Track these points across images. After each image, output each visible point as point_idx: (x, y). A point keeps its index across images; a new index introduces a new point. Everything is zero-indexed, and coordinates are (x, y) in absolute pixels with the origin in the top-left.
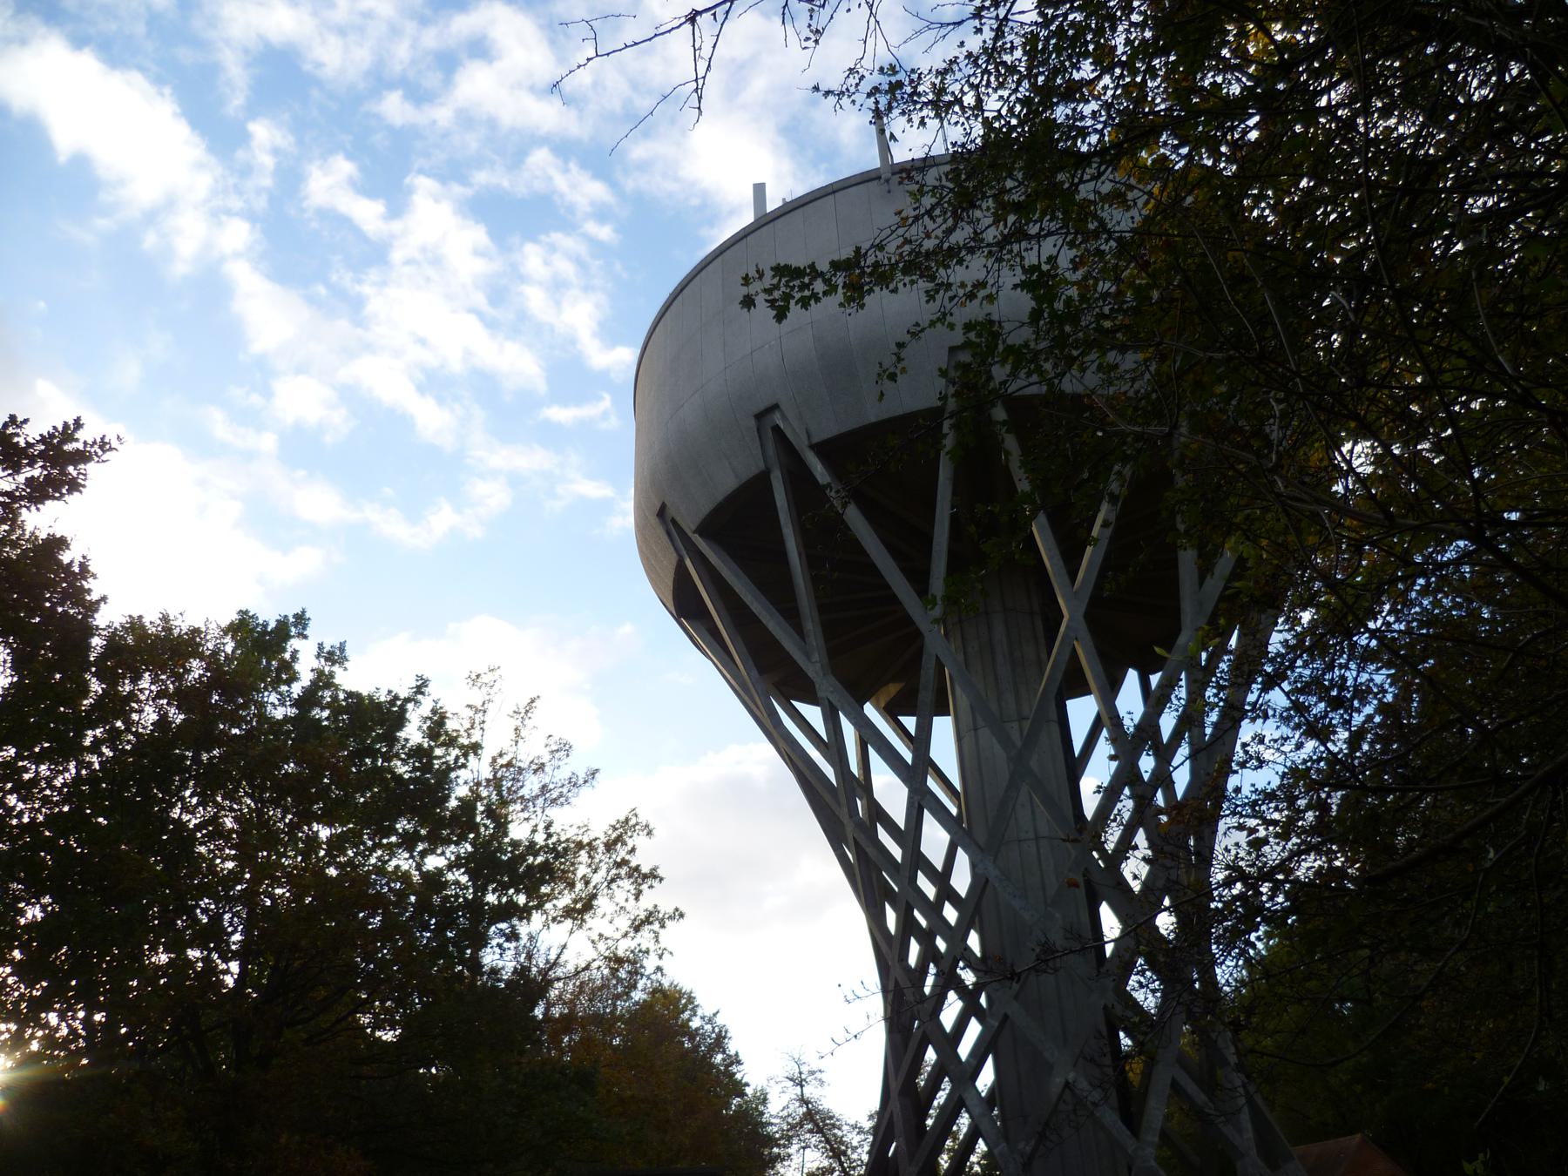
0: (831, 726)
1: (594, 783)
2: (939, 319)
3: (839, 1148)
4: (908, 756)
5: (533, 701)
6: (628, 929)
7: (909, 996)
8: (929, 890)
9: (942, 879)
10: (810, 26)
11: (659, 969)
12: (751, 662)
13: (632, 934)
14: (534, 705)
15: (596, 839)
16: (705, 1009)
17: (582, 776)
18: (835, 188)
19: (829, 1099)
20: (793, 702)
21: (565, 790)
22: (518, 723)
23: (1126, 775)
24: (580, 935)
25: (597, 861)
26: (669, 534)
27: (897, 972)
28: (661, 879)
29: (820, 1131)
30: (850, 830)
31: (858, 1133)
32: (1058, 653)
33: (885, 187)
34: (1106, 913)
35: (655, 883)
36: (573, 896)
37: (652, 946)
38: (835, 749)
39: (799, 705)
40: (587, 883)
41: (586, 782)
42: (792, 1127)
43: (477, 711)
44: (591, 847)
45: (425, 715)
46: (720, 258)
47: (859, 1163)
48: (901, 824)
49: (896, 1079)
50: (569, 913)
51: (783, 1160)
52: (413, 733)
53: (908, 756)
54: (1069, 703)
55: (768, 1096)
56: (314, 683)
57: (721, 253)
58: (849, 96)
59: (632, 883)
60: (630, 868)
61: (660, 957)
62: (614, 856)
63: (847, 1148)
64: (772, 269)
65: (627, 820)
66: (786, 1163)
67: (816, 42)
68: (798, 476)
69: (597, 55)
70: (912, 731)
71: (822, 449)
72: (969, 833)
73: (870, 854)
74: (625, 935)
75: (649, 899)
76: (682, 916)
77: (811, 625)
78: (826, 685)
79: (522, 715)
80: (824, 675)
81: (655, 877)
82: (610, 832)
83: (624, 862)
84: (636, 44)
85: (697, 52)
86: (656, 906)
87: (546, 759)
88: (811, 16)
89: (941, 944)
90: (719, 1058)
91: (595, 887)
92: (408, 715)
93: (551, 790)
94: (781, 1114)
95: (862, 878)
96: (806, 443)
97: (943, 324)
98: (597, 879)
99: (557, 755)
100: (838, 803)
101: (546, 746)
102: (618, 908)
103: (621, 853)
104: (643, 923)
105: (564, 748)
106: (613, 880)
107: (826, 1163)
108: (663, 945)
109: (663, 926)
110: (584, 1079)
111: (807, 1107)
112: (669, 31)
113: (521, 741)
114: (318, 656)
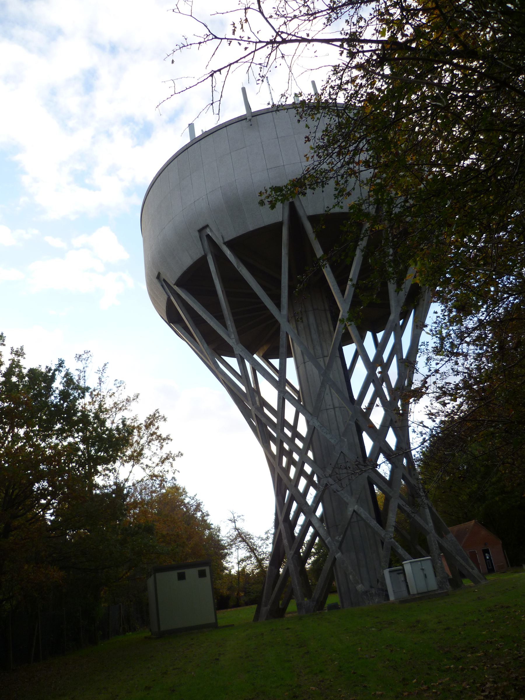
0: (242, 366)
1: (138, 400)
2: (336, 205)
3: (253, 547)
5: (105, 365)
6: (159, 462)
8: (289, 434)
9: (294, 428)
10: (259, 74)
12: (203, 340)
13: (161, 464)
14: (106, 367)
16: (190, 494)
17: (132, 397)
18: (226, 124)
19: (246, 527)
20: (223, 357)
21: (124, 403)
22: (100, 375)
23: (370, 379)
24: (137, 466)
26: (162, 286)
27: (278, 470)
28: (171, 440)
29: (244, 540)
30: (253, 412)
32: (339, 327)
34: (365, 436)
35: (169, 442)
36: (133, 450)
38: (244, 378)
39: (225, 358)
40: (138, 443)
41: (134, 400)
42: (232, 541)
43: (81, 372)
44: (139, 428)
46: (176, 159)
47: (262, 552)
49: (281, 516)
50: (131, 457)
51: (229, 555)
52: (58, 385)
54: (344, 348)
55: (221, 528)
56: (11, 365)
57: (177, 157)
61: (174, 473)
62: (150, 431)
64: (270, 188)
65: (155, 415)
66: (230, 556)
68: (220, 257)
70: (278, 367)
71: (230, 244)
72: (304, 407)
74: (157, 465)
75: (168, 448)
76: (182, 455)
77: (230, 322)
78: (238, 348)
79: (101, 371)
81: (169, 439)
83: (154, 433)
84: (190, 87)
85: (213, 88)
87: (114, 390)
88: (261, 71)
89: (296, 457)
90: (199, 514)
92: (56, 377)
93: (118, 404)
94: (227, 536)
95: (261, 434)
96: (222, 242)
98: (142, 441)
102: (153, 454)
103: (153, 429)
105: (119, 384)
106: (150, 442)
107: (248, 554)
108: (174, 468)
109: (174, 460)
110: (149, 529)
111: (238, 531)
112: (203, 81)
113: (102, 383)
114: (12, 353)
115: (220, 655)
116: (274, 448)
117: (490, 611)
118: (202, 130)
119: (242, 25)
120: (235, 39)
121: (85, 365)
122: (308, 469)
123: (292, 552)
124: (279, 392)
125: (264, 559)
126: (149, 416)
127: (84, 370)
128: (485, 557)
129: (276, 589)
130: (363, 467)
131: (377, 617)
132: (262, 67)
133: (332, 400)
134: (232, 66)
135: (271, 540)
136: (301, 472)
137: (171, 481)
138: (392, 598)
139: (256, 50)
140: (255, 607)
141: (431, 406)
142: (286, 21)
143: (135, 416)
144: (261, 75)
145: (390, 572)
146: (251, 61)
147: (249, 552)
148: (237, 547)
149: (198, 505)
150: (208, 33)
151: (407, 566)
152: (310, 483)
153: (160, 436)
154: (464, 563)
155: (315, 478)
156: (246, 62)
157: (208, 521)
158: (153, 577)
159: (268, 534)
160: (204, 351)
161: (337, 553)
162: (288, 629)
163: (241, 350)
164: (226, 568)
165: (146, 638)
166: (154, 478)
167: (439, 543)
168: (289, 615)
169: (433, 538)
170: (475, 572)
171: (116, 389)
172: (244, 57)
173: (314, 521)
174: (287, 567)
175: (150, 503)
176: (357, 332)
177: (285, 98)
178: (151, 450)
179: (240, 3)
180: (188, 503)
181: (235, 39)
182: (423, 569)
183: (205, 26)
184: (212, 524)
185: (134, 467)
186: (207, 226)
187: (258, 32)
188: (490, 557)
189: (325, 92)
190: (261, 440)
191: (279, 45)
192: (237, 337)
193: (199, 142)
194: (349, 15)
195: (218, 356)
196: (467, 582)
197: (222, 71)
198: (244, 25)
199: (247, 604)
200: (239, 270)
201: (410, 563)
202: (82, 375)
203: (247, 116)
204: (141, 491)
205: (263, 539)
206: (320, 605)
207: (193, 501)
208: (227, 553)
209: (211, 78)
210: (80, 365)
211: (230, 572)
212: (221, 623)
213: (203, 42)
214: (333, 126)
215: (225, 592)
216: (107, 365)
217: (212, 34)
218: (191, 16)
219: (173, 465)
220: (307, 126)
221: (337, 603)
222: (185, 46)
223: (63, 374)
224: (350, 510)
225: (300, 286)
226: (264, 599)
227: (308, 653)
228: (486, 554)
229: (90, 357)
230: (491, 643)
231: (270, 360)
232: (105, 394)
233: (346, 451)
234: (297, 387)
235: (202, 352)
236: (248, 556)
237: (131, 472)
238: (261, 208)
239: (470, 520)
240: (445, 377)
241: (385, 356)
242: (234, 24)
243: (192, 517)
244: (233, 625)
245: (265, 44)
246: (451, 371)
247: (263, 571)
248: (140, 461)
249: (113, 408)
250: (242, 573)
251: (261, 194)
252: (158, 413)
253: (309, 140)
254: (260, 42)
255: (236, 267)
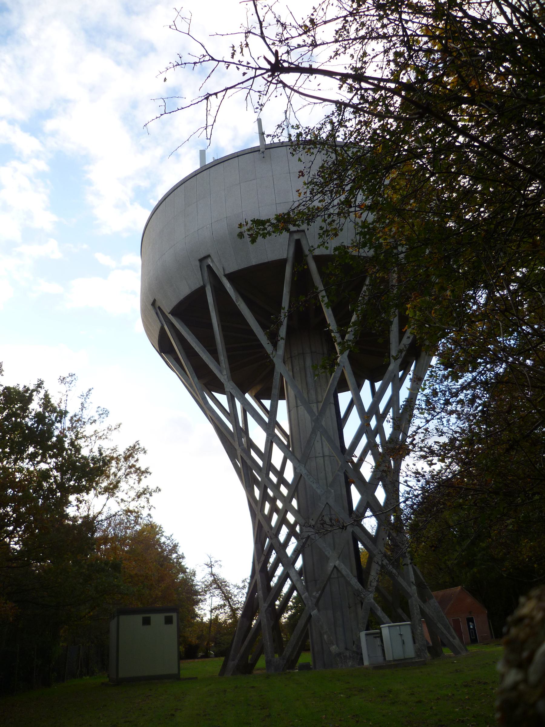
2: (322, 245)
3: (228, 596)
4: (267, 420)
5: (90, 390)
7: (266, 528)
8: (274, 478)
9: (280, 474)
11: (149, 515)
12: (194, 374)
13: (136, 499)
14: (90, 392)
15: (120, 455)
18: (238, 154)
19: (222, 574)
22: (83, 400)
23: (364, 429)
24: (112, 500)
25: (120, 465)
26: (157, 314)
27: (259, 517)
28: (150, 474)
29: (219, 587)
31: (237, 589)
33: (262, 155)
34: (354, 489)
35: (148, 475)
36: (109, 482)
37: (145, 504)
38: (232, 416)
39: (215, 394)
40: (115, 476)
41: (115, 429)
42: (207, 586)
44: (117, 459)
45: (41, 397)
47: (237, 602)
48: (263, 450)
50: (106, 489)
51: (202, 601)
52: (35, 406)
53: (267, 420)
55: (196, 573)
57: (184, 183)
58: (278, 138)
59: (137, 475)
60: (136, 468)
61: (150, 509)
62: (128, 463)
63: (232, 595)
64: (251, 221)
65: (135, 446)
66: (204, 603)
67: (261, 109)
68: (219, 289)
69: (165, 113)
70: (269, 408)
71: (230, 277)
72: (293, 453)
73: (248, 463)
74: (133, 500)
75: (146, 482)
76: (160, 490)
77: (223, 357)
78: (229, 385)
80: (229, 381)
81: (147, 472)
82: (126, 452)
83: (133, 466)
85: (208, 112)
86: (147, 486)
87: (96, 417)
88: (260, 98)
89: (280, 504)
90: (174, 556)
91: (119, 477)
92: (33, 398)
94: (202, 580)
96: (223, 273)
97: (323, 247)
98: (120, 474)
99: (102, 416)
100: (234, 440)
101: (97, 411)
103: (132, 461)
104: (141, 494)
105: (105, 413)
106: (128, 474)
107: (222, 602)
108: (151, 504)
109: (151, 495)
110: (116, 567)
111: (214, 578)
112: (197, 103)
113: (84, 409)
115: (176, 710)
116: (257, 493)
117: (466, 686)
118: (214, 158)
119: (242, 49)
120: (234, 63)
121: (68, 389)
122: (291, 518)
123: (266, 605)
124: (267, 435)
125: (238, 608)
126: (128, 448)
127: (66, 394)
128: (469, 626)
129: (246, 643)
130: (329, 527)
131: (348, 683)
132: (262, 95)
133: (322, 447)
134: (228, 90)
135: (246, 590)
136: (283, 520)
137: (147, 518)
138: (366, 663)
139: (255, 77)
140: (223, 659)
141: (407, 467)
142: (289, 49)
143: (115, 446)
144: (260, 103)
145: (366, 635)
146: (249, 88)
147: (224, 600)
148: (212, 594)
149: (175, 546)
150: (205, 54)
151: (385, 630)
152: (292, 533)
153: (139, 469)
154: (445, 632)
155: (298, 529)
156: (244, 88)
157: (183, 564)
158: (116, 619)
159: (245, 583)
160: (194, 385)
161: (313, 610)
162: (253, 687)
163: (231, 387)
164: (197, 615)
165: (103, 684)
166: (129, 514)
167: (420, 607)
168: (258, 672)
169: (415, 600)
170: (456, 642)
171: (98, 417)
172: (242, 83)
173: (292, 574)
174: (259, 621)
175: (123, 540)
176: (354, 380)
177: (281, 129)
178: (129, 483)
179: (242, 26)
180: (164, 543)
181: (234, 63)
182: (401, 635)
183: (202, 46)
184: (187, 568)
185: (109, 500)
186: (209, 256)
187: (258, 58)
188: (474, 627)
189: (324, 126)
190: (244, 483)
191: (279, 74)
192: (229, 374)
193: (208, 170)
194: (354, 49)
195: (208, 391)
196: (447, 651)
197: (218, 94)
198: (245, 49)
199: (216, 656)
200: (237, 304)
201: (389, 627)
202: (64, 398)
203: (261, 147)
204: (116, 526)
205: (239, 588)
206: (291, 664)
207: (169, 541)
208: (201, 599)
209: (205, 101)
210: (63, 388)
211: (202, 620)
212: (184, 674)
213: (198, 63)
214: (330, 163)
215: (194, 640)
216: (92, 390)
217: (209, 55)
218: (188, 34)
219: (149, 501)
220: (300, 160)
221: (309, 663)
222: (179, 65)
223: (42, 395)
224: (331, 565)
225: (273, 326)
226: (232, 652)
227: (269, 716)
228: (471, 623)
229: (74, 381)
230: (463, 721)
231: (262, 401)
232: (86, 420)
233: (331, 502)
234: (287, 430)
235: (191, 386)
236: (221, 604)
237: (105, 505)
238: (239, 239)
239: (456, 586)
240: (428, 436)
241: (382, 406)
242: (233, 47)
243: (167, 559)
244: (196, 678)
245: (265, 71)
246: (435, 431)
247: (235, 621)
248: (115, 494)
249: (92, 435)
250: (214, 622)
251: (241, 225)
252: (139, 444)
253: (303, 175)
254: (260, 68)
255: (235, 300)
